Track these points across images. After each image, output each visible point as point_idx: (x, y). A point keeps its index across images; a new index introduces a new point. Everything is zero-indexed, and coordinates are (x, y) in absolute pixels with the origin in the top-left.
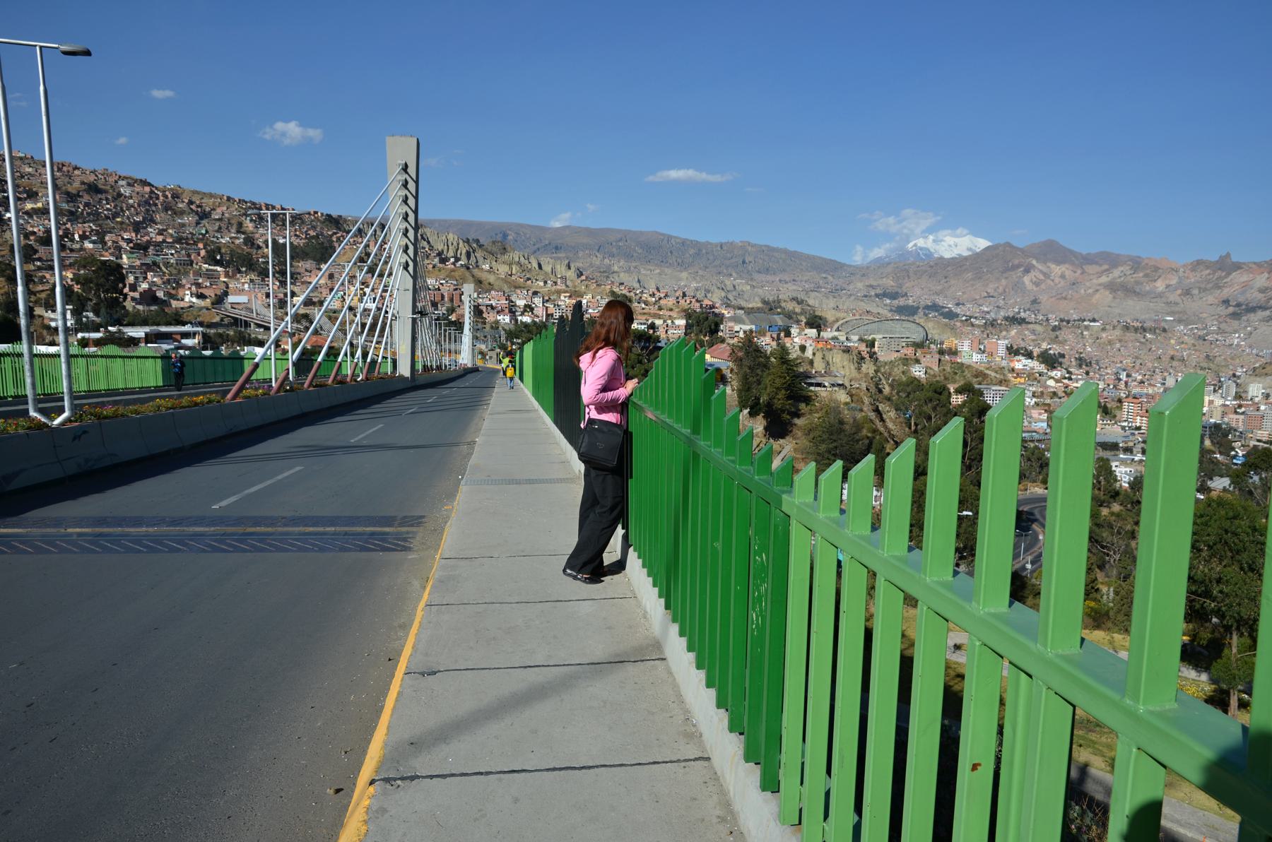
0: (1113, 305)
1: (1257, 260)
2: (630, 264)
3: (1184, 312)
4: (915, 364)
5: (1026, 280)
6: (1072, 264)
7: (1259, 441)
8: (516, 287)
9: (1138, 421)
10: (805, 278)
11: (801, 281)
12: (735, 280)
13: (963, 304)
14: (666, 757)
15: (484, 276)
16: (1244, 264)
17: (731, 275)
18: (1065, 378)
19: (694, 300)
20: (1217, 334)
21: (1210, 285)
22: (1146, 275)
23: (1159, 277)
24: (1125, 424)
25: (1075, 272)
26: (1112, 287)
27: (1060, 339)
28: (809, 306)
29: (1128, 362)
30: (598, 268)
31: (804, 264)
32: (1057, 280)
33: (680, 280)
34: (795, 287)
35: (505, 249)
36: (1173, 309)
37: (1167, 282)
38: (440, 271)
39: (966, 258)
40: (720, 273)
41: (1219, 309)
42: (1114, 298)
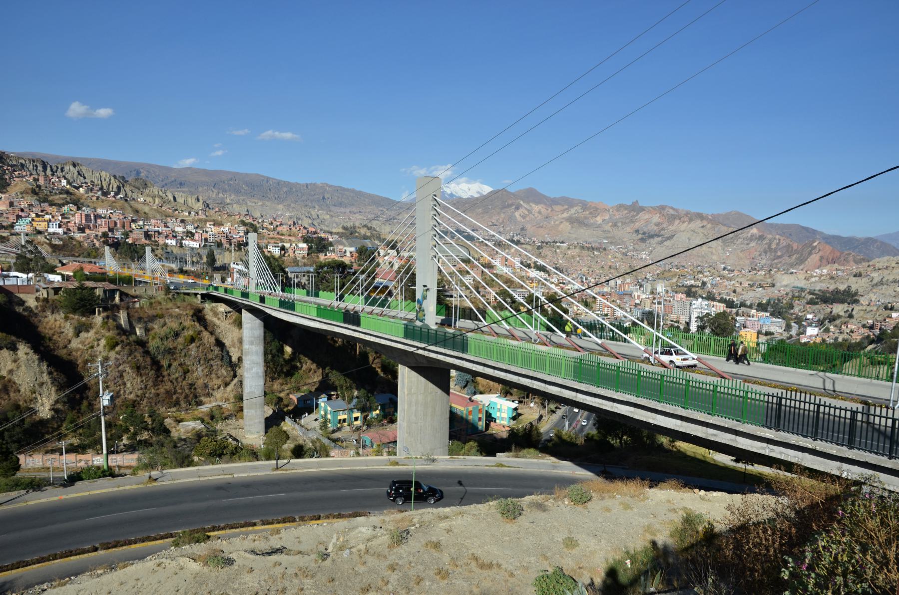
0: (571, 232)
1: (653, 206)
2: (239, 198)
3: (614, 237)
4: (466, 274)
5: (517, 214)
6: (545, 204)
7: (672, 321)
8: (166, 216)
9: (606, 310)
10: (368, 211)
11: (365, 212)
12: (318, 211)
13: (477, 230)
14: (702, 498)
15: (139, 207)
16: (646, 207)
17: (315, 207)
18: (561, 283)
19: (302, 228)
20: (633, 252)
21: (628, 220)
22: (591, 213)
23: (599, 214)
24: (599, 312)
25: (547, 210)
26: (571, 220)
27: (543, 254)
28: (376, 231)
29: (585, 269)
30: (214, 200)
31: (367, 200)
32: (536, 215)
33: (278, 210)
34: (361, 217)
35: (146, 184)
36: (607, 235)
37: (603, 218)
38: (103, 202)
39: (477, 199)
40: (306, 206)
41: (634, 235)
42: (572, 227)
